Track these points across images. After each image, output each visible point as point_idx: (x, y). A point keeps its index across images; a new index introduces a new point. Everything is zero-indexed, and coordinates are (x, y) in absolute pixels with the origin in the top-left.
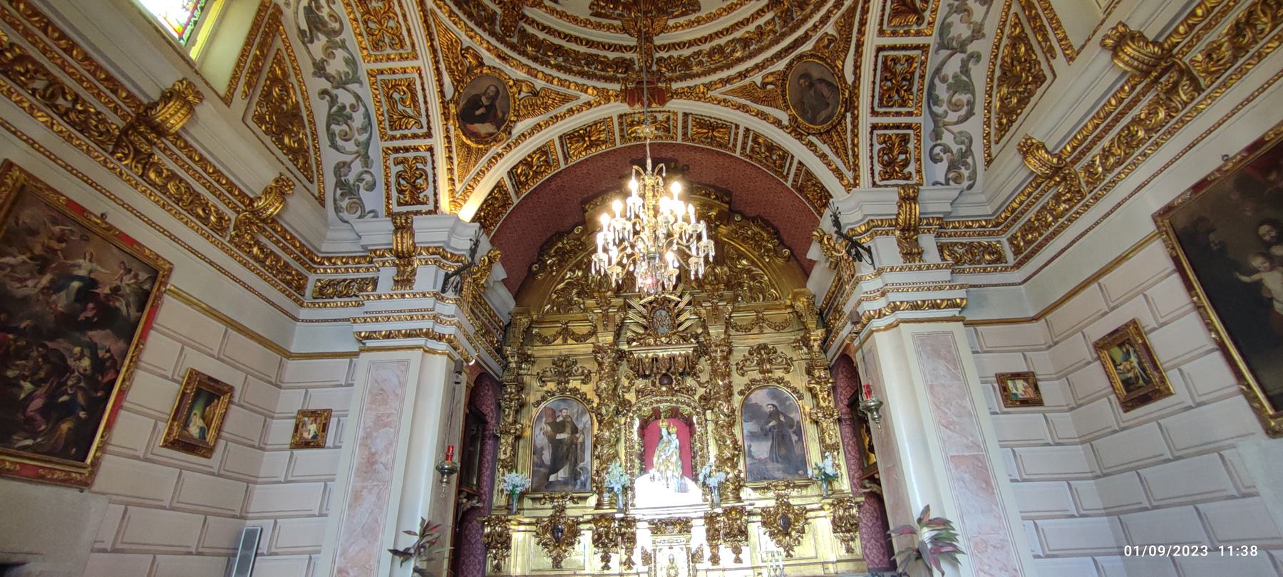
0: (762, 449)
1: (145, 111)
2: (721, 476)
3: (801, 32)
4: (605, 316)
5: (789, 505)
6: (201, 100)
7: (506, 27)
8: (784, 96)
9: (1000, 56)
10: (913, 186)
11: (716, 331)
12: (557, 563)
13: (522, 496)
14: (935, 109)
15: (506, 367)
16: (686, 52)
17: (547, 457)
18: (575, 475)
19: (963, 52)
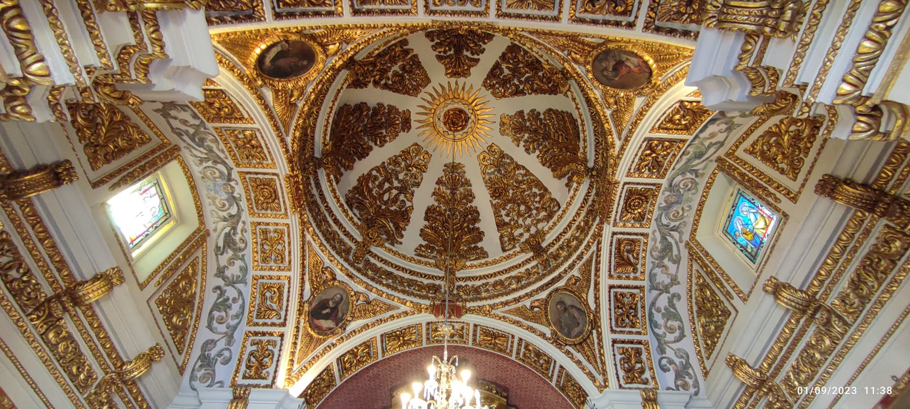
1: (75, 287)
3: (556, 274)
6: (122, 283)
7: (356, 257)
8: (547, 316)
9: (693, 296)
10: (651, 390)
14: (656, 330)
16: (478, 283)
19: (668, 292)
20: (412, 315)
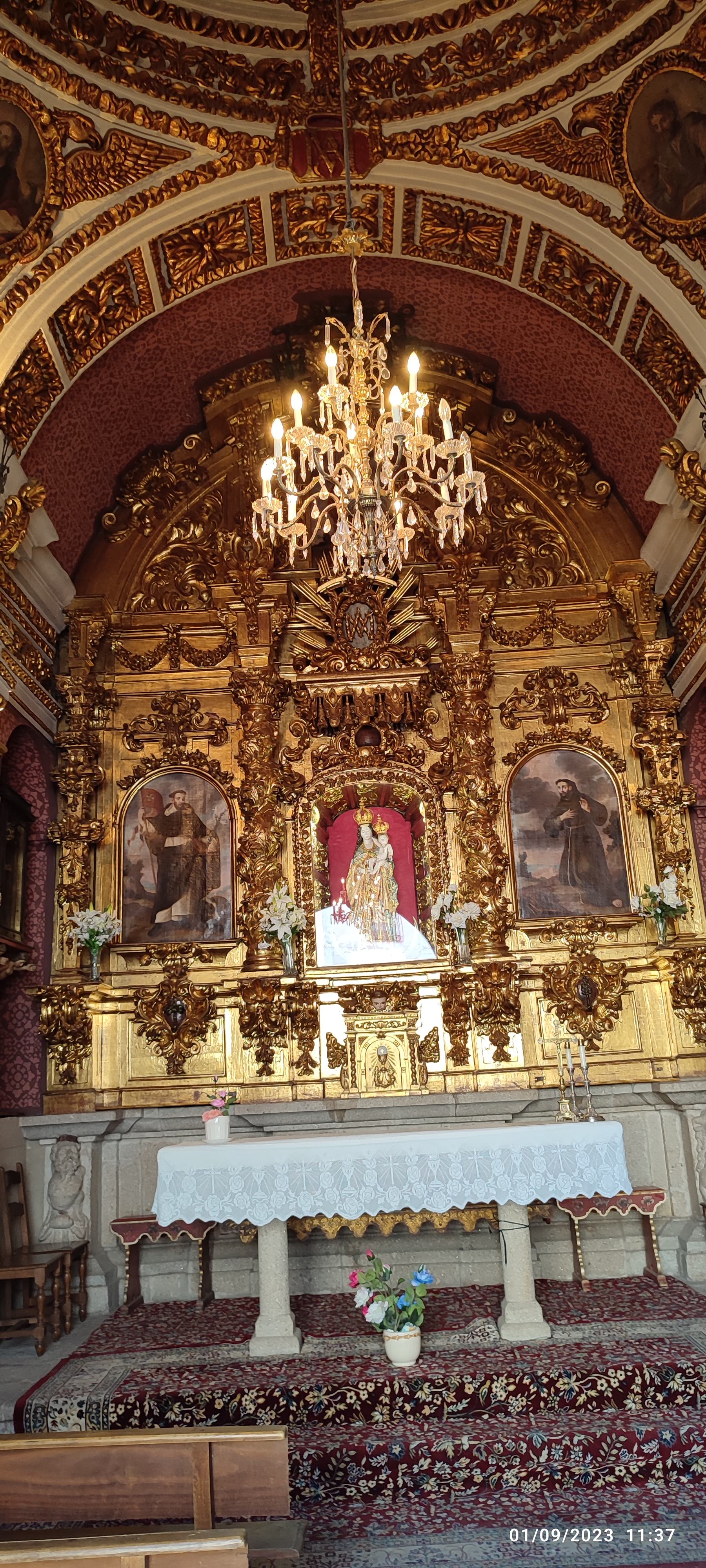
0: (545, 862)
2: (472, 910)
4: (252, 615)
5: (593, 960)
8: (617, 152)
11: (464, 645)
12: (175, 1067)
13: (107, 949)
15: (63, 713)
16: (415, 48)
17: (149, 879)
18: (202, 912)
20: (230, 179)
